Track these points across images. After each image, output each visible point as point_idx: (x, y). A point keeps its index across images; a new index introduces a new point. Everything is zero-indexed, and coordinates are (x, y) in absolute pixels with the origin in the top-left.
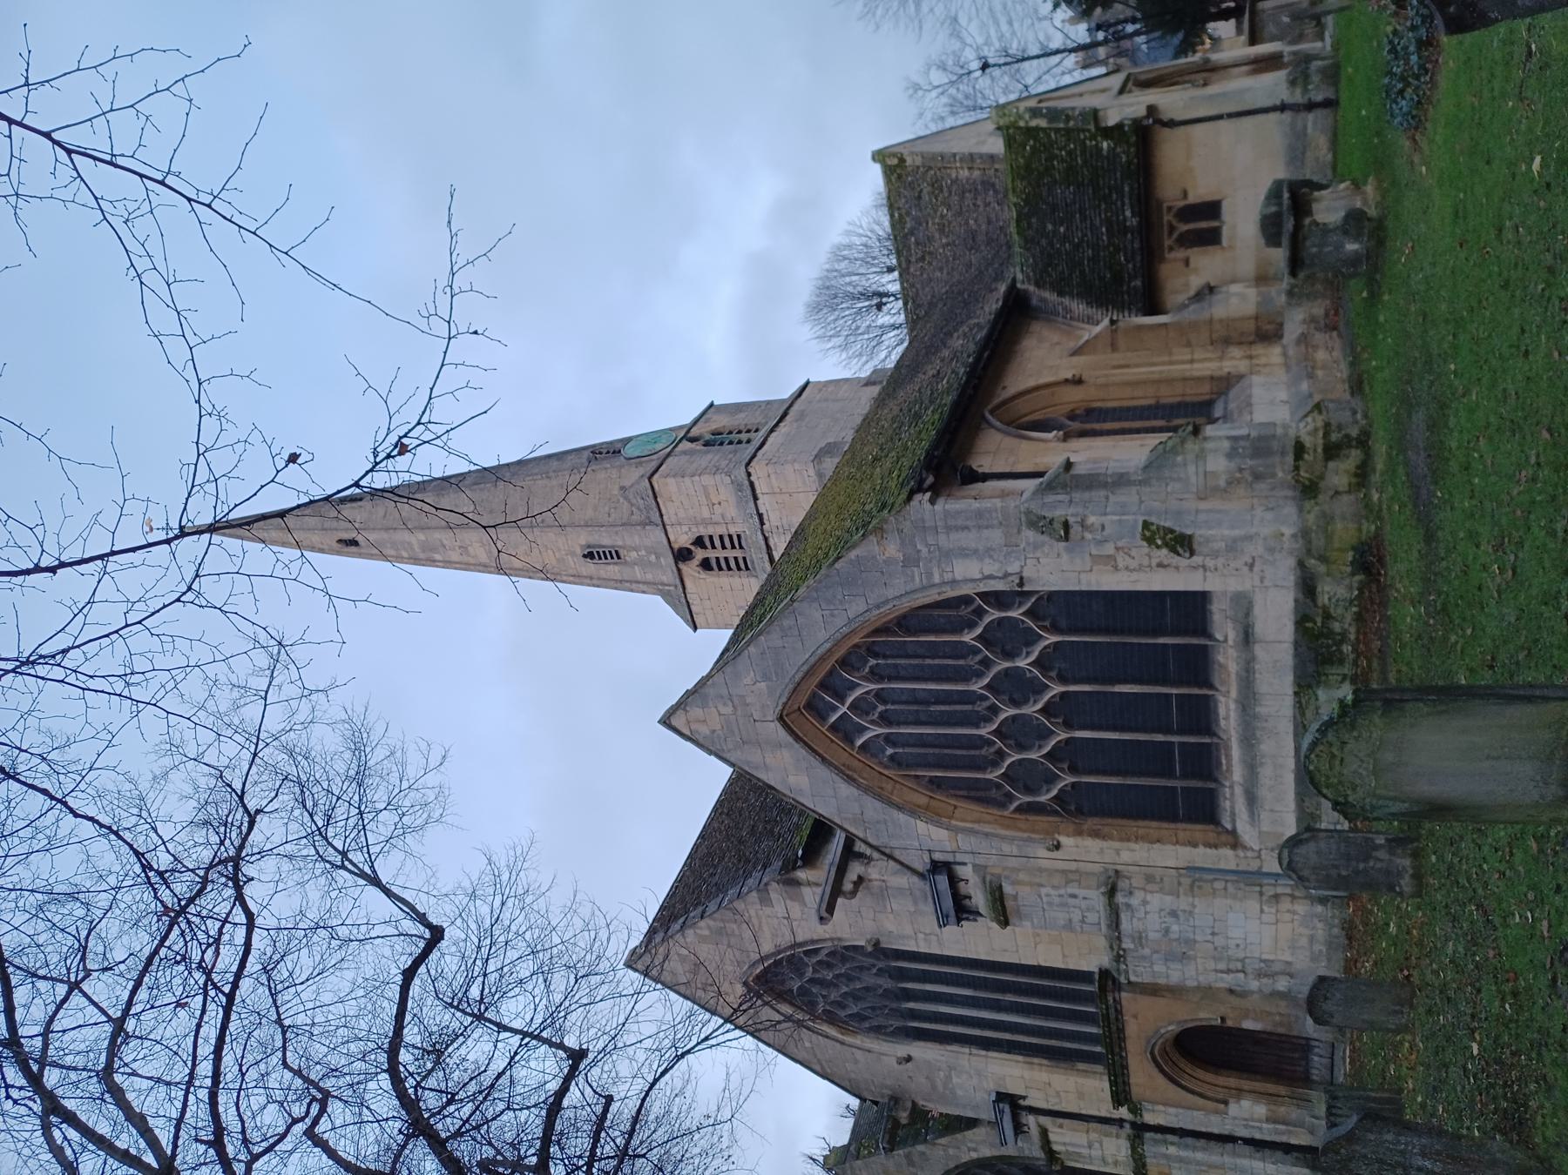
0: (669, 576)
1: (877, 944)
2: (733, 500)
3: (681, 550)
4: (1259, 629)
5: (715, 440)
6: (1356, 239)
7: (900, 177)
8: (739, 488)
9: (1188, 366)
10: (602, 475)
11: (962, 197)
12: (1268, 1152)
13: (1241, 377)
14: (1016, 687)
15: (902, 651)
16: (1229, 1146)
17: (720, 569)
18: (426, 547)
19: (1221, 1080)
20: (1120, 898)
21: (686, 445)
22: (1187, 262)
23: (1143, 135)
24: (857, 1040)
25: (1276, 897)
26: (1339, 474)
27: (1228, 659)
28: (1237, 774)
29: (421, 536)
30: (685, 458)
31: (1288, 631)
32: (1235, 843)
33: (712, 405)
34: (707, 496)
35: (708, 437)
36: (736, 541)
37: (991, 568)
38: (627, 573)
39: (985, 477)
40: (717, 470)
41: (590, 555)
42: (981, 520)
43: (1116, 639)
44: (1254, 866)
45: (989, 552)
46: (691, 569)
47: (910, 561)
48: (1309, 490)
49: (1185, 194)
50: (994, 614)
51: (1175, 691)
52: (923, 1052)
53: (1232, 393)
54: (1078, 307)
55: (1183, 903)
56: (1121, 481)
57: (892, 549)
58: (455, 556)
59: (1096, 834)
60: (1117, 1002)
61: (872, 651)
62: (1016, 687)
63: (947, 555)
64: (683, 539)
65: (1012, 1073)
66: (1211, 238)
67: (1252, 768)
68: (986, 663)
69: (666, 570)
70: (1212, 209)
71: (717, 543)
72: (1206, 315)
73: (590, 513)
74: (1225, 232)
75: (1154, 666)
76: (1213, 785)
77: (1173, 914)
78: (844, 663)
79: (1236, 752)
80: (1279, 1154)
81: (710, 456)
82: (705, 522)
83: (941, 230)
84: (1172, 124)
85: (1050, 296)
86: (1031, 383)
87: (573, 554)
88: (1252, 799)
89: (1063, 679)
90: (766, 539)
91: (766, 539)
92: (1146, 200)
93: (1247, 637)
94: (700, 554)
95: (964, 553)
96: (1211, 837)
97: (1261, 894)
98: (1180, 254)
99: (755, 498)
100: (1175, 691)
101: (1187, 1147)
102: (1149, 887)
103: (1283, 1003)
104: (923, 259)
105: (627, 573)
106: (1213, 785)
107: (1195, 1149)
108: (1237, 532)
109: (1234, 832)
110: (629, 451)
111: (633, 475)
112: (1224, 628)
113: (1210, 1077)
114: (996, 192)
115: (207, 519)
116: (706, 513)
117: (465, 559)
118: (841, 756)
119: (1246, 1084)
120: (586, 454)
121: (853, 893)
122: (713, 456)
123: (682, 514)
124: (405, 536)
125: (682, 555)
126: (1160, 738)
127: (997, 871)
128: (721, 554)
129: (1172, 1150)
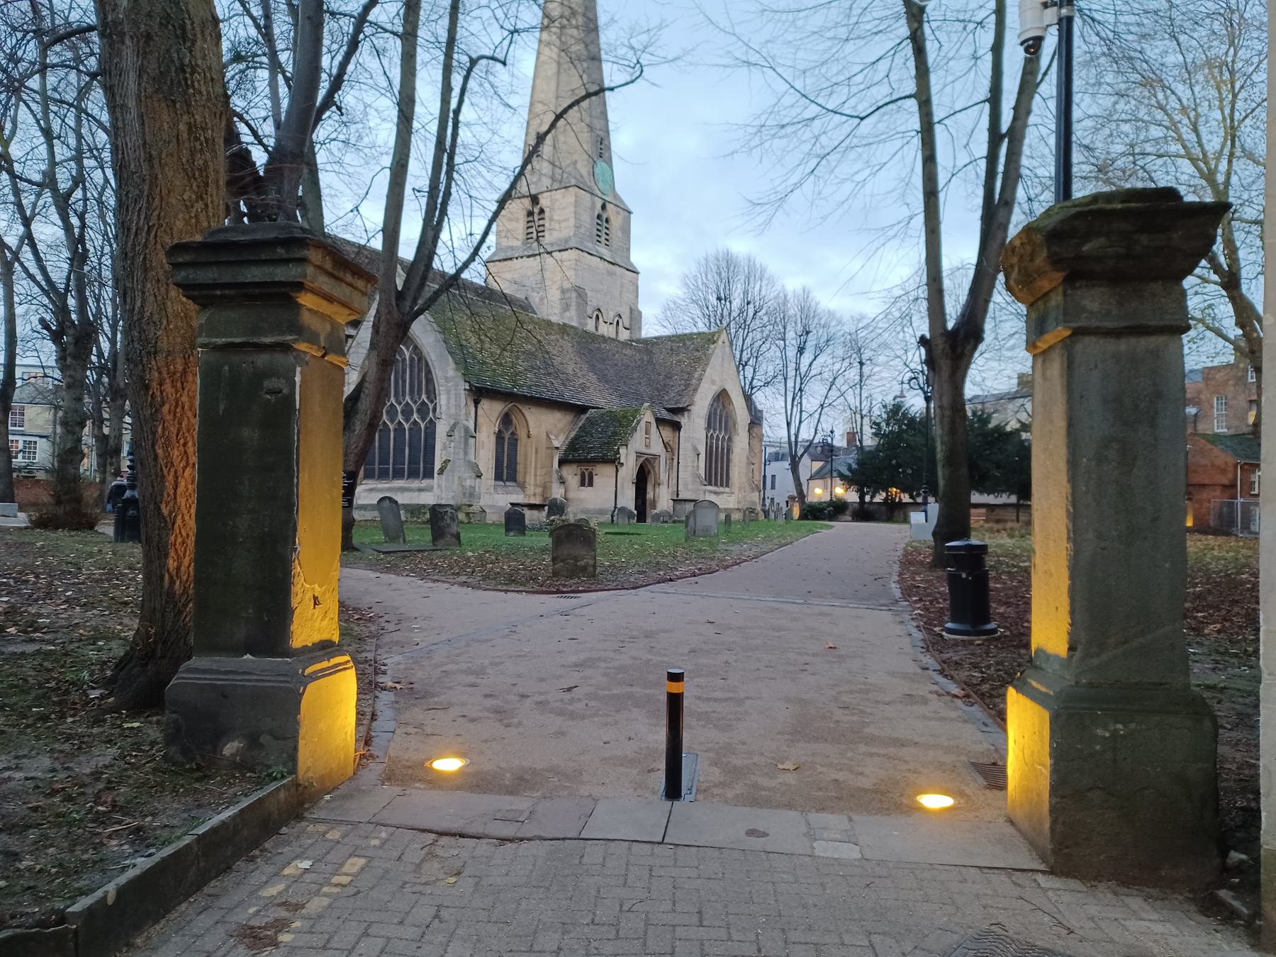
4: (423, 494)
5: (602, 220)
14: (407, 413)
15: (420, 370)
21: (599, 203)
23: (614, 461)
27: (415, 484)
28: (380, 486)
30: (589, 204)
31: (422, 502)
37: (444, 408)
39: (476, 407)
40: (577, 227)
42: (458, 406)
47: (446, 379)
50: (431, 406)
54: (572, 435)
56: (466, 453)
57: (451, 373)
61: (420, 359)
62: (407, 413)
63: (448, 393)
64: (544, 201)
66: (583, 484)
68: (415, 402)
70: (591, 484)
75: (414, 461)
78: (416, 347)
81: (589, 220)
83: (679, 361)
88: (371, 490)
89: (410, 429)
92: (594, 461)
93: (421, 490)
95: (448, 400)
110: (601, 165)
111: (583, 169)
112: (425, 483)
122: (588, 220)
125: (535, 199)
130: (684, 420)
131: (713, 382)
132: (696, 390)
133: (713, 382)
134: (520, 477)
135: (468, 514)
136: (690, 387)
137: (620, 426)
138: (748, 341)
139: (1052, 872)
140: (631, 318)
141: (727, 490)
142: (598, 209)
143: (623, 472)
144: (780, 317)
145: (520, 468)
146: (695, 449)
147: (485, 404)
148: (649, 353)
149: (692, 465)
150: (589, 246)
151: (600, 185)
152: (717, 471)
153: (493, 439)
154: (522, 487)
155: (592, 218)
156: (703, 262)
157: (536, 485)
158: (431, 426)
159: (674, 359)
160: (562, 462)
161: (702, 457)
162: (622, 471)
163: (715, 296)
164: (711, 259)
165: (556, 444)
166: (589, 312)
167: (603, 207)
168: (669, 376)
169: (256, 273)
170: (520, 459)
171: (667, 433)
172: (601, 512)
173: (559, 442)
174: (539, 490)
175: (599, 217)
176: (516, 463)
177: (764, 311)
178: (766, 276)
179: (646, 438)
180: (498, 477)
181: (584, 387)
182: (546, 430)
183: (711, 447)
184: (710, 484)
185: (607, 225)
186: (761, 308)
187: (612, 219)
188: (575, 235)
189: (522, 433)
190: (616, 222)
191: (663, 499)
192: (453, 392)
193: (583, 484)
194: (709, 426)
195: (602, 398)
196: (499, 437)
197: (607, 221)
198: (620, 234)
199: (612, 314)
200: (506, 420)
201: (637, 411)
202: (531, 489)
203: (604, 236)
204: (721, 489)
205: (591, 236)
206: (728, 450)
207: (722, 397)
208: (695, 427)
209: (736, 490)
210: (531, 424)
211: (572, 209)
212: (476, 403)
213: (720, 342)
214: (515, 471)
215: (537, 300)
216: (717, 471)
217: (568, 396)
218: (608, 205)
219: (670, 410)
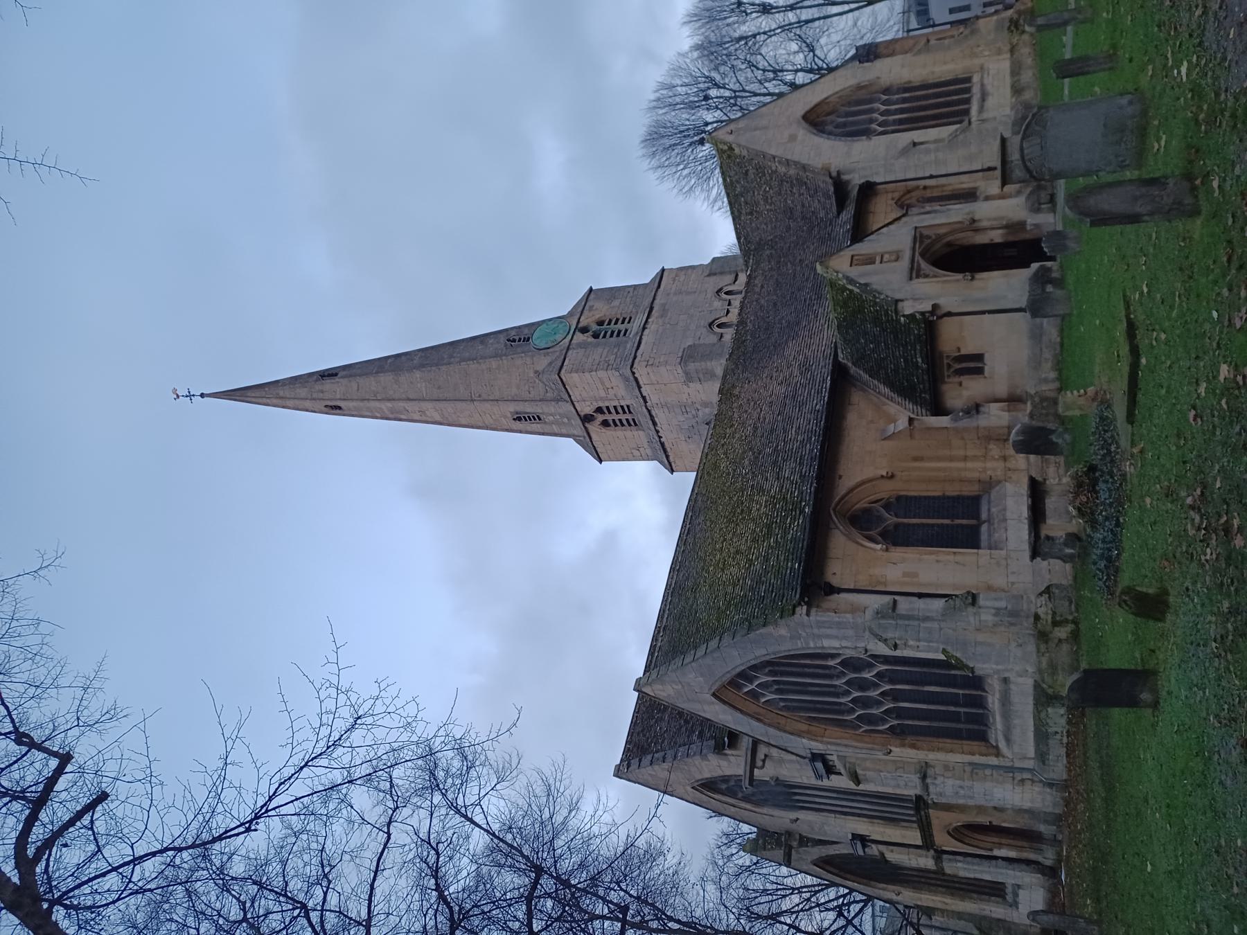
0: (579, 430)
1: (777, 779)
2: (622, 386)
3: (586, 416)
6: (1072, 548)
7: (729, 157)
8: (627, 380)
9: (961, 465)
10: (519, 362)
11: (781, 185)
12: (1016, 865)
13: (999, 482)
16: (994, 862)
17: (616, 425)
18: (392, 411)
19: (989, 839)
20: (929, 781)
21: (579, 337)
22: (960, 384)
23: (930, 323)
24: (765, 810)
25: (1023, 781)
26: (1062, 632)
29: (389, 404)
32: (998, 754)
33: (591, 290)
34: (603, 383)
35: (595, 327)
36: (627, 409)
38: (547, 428)
39: (840, 591)
41: (519, 419)
42: (840, 625)
43: (925, 670)
44: (1009, 764)
45: (845, 638)
46: (594, 428)
48: (1043, 636)
49: (959, 350)
51: (961, 692)
52: (802, 815)
53: (994, 494)
55: (967, 783)
57: (783, 631)
58: (416, 417)
59: (913, 746)
60: (928, 816)
62: (863, 685)
63: (820, 637)
64: (587, 409)
65: (863, 827)
66: (979, 371)
67: (1006, 716)
69: (578, 428)
70: (979, 357)
71: (613, 410)
72: (975, 424)
73: (514, 391)
74: (986, 368)
76: (982, 728)
77: (961, 787)
79: (998, 718)
80: (1024, 867)
81: (600, 350)
82: (602, 399)
83: (766, 200)
84: (949, 314)
85: (866, 377)
86: (859, 479)
87: (505, 417)
90: (649, 411)
91: (649, 411)
94: (600, 418)
95: (828, 637)
96: (983, 749)
97: (1014, 778)
98: (957, 379)
99: (639, 387)
100: (961, 692)
101: (968, 863)
102: (946, 774)
103: (1026, 816)
104: (751, 213)
105: (547, 428)
106: (982, 728)
107: (973, 864)
108: (1000, 667)
109: (997, 747)
110: (538, 340)
111: (542, 362)
113: (983, 838)
114: (808, 189)
115: (645, 394)
116: (603, 394)
117: (424, 418)
118: (752, 708)
119: (1004, 841)
120: (502, 338)
121: (763, 767)
122: (600, 351)
123: (584, 394)
124: (377, 404)
125: (587, 419)
126: (952, 709)
127: (853, 760)
128: (617, 417)
129: (959, 865)
130: (856, 180)
131: (793, 138)
132: (804, 168)
133: (793, 138)
134: (969, 490)
135: (1055, 624)
136: (800, 177)
137: (864, 316)
138: (754, 87)
139: (876, 184)
140: (722, 273)
141: (976, 79)
142: (587, 338)
143: (949, 302)
144: (711, 50)
145: (952, 490)
146: (904, 152)
147: (837, 572)
148: (760, 246)
149: (935, 153)
150: (630, 346)
151: (559, 337)
152: (944, 103)
153: (898, 553)
154: (989, 485)
155: (598, 345)
156: (660, 171)
157: (985, 457)
158: (886, 660)
159: (762, 207)
160: (938, 409)
161: (917, 135)
162: (948, 304)
163: (700, 148)
164: (654, 162)
165: (902, 424)
166: (713, 339)
167: (584, 330)
168: (789, 213)
169: (729, 718)
170: (935, 491)
171: (882, 209)
172: (1036, 336)
173: (900, 414)
174: (995, 450)
175: (596, 336)
176: (944, 498)
177: (714, 74)
178: (668, 81)
179: (885, 266)
180: (969, 539)
181: (805, 368)
182: (883, 444)
183: (901, 122)
184: (967, 112)
185: (605, 322)
186: (712, 80)
187: (598, 316)
188: (617, 369)
189: (887, 490)
190: (601, 310)
191: (1000, 210)
192: (816, 631)
193: (979, 371)
194: (867, 133)
195: (822, 337)
196: (896, 538)
197: (600, 323)
198: (616, 303)
199: (717, 304)
200: (862, 521)
201: (832, 284)
202: (994, 468)
203: (619, 326)
204: (976, 90)
205: (618, 345)
206: (906, 90)
207: (816, 120)
208: (866, 158)
209: (977, 62)
210: (869, 473)
211: (587, 374)
212: (832, 590)
213: (730, 138)
214: (958, 499)
215: (707, 410)
216: (944, 103)
217: (818, 402)
218: (581, 325)
219: (841, 205)
